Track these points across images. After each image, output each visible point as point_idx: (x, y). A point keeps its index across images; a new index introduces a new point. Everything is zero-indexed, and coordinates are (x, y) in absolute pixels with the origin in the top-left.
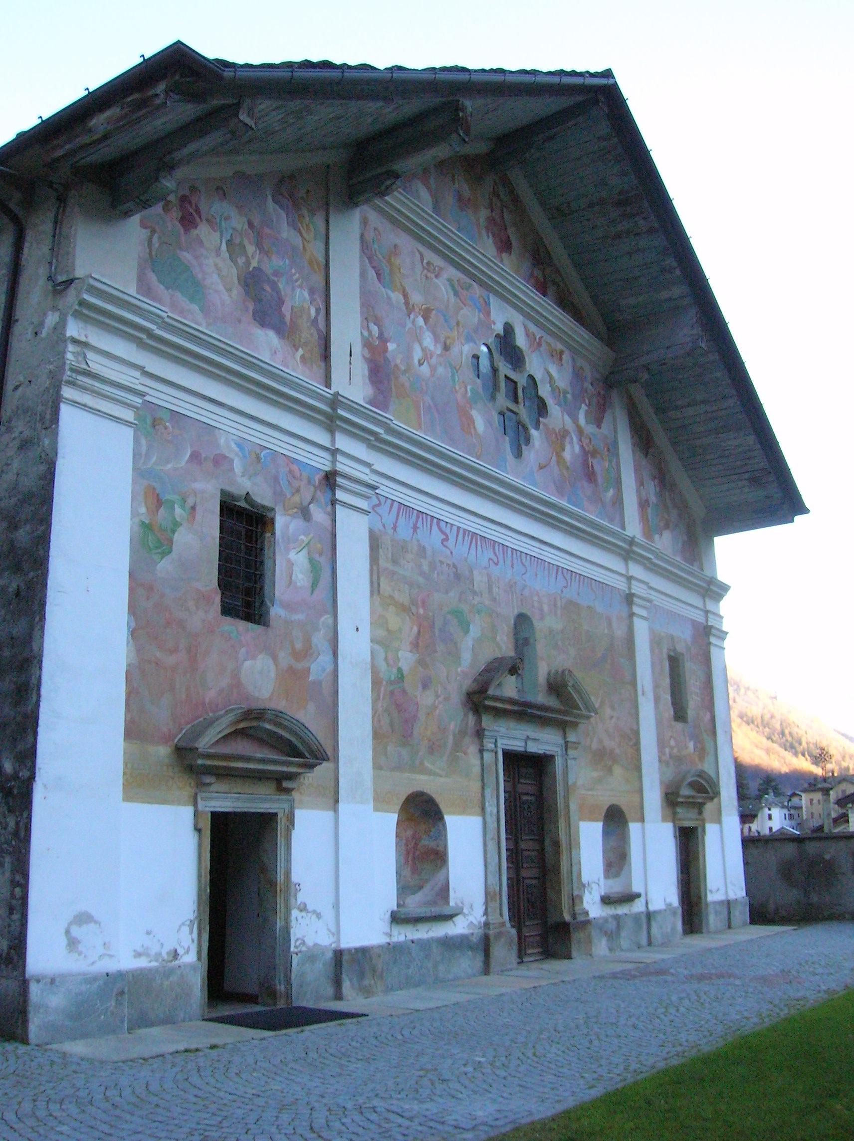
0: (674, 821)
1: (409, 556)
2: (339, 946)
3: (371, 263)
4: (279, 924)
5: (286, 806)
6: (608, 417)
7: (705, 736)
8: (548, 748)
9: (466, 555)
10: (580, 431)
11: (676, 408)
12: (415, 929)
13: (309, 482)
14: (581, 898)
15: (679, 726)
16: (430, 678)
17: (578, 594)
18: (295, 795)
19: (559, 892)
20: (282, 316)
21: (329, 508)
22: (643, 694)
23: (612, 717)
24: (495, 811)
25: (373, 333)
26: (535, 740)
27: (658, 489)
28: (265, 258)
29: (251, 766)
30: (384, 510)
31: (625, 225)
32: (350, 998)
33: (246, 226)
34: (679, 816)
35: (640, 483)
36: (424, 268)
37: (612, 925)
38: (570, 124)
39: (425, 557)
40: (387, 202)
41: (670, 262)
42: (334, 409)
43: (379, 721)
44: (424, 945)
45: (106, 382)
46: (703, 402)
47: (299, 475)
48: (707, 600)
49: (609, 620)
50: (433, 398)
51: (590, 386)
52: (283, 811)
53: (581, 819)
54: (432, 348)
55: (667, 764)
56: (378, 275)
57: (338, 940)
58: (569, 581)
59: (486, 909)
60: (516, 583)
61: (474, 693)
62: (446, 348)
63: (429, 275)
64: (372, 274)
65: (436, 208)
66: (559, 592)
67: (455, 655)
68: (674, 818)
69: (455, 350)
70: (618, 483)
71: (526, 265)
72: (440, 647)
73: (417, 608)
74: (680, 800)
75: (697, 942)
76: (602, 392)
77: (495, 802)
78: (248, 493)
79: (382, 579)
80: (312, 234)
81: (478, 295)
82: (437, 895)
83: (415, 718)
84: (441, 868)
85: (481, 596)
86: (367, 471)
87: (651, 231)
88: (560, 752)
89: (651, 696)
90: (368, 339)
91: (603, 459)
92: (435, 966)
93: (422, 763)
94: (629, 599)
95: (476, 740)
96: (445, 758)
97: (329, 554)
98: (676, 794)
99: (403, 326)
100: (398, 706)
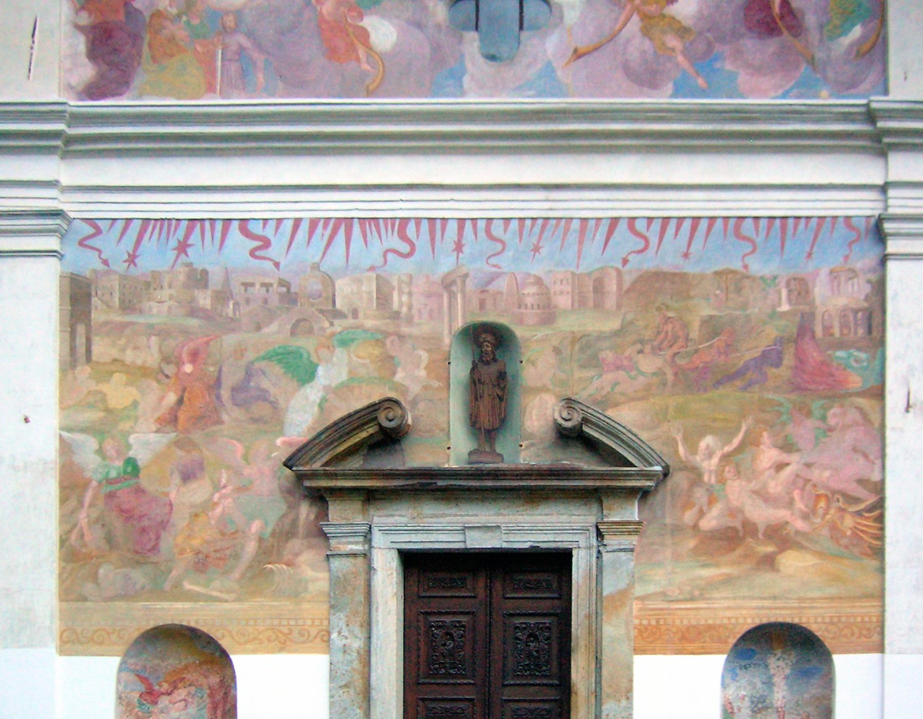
1: (165, 294)
45: (32, 215)
58: (654, 241)
60: (466, 275)
66: (619, 265)
72: (231, 415)
83: (164, 525)
86: (53, 193)
93: (177, 585)
95: (318, 541)
96: (236, 575)
100: (127, 514)
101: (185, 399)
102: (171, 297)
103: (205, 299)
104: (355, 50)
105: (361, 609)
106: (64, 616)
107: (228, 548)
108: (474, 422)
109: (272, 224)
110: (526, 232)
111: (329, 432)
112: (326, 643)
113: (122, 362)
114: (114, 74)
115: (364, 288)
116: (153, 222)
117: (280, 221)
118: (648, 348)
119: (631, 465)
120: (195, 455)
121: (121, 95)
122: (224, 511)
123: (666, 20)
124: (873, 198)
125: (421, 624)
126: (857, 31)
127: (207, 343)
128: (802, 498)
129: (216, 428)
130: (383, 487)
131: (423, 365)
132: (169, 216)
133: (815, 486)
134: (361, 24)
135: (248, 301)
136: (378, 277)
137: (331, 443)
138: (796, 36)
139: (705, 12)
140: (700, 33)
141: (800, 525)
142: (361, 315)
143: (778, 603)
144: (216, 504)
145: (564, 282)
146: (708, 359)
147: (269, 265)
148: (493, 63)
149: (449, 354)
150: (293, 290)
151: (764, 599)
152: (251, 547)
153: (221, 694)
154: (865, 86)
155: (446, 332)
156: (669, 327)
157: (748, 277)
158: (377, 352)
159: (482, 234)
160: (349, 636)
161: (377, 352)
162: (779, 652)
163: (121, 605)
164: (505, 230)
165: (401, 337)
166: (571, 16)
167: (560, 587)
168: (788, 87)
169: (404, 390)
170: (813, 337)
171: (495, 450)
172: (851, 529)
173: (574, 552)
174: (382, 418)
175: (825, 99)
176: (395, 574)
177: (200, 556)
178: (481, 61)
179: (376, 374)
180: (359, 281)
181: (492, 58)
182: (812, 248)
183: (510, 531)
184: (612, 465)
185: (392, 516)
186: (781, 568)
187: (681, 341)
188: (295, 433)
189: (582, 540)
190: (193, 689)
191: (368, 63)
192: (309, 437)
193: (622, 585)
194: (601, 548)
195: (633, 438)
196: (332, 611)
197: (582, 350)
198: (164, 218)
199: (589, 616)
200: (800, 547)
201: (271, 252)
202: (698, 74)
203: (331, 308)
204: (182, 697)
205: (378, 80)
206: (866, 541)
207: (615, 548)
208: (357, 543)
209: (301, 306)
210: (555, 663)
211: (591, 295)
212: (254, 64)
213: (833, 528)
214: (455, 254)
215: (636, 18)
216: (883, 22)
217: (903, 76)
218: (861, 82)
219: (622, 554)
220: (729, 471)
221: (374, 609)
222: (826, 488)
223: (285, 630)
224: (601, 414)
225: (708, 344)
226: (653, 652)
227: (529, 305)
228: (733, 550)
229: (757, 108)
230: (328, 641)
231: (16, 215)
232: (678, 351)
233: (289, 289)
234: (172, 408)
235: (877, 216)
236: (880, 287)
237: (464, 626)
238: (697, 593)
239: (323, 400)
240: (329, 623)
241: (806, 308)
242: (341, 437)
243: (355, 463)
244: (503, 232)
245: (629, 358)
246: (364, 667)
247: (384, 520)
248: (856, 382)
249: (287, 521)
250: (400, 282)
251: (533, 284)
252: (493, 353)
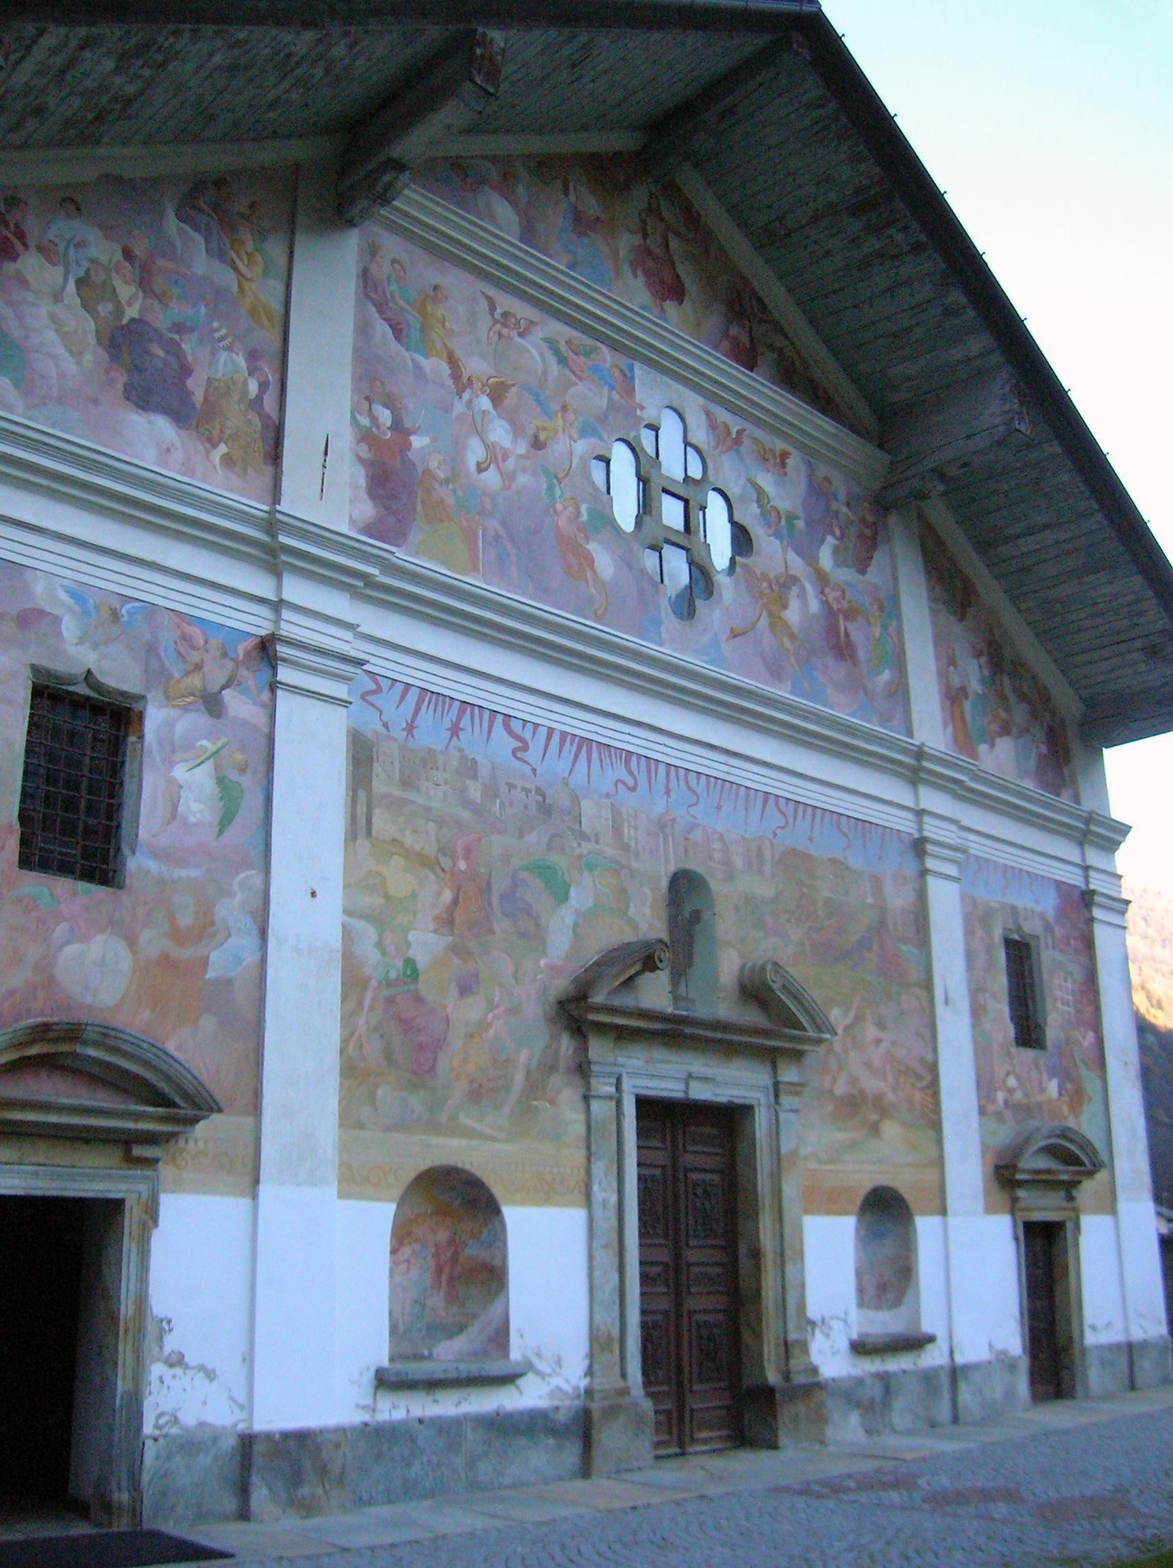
0: (1012, 1212)
1: (440, 776)
2: (252, 1428)
3: (381, 312)
4: (121, 1386)
5: (143, 1188)
6: (880, 558)
7: (1083, 1071)
8: (741, 1093)
9: (566, 775)
10: (822, 579)
11: (1007, 540)
12: (430, 1398)
13: (225, 654)
14: (804, 1347)
15: (1028, 1054)
16: (477, 976)
17: (811, 839)
18: (166, 1171)
19: (758, 1336)
20: (186, 395)
21: (265, 696)
22: (947, 1002)
23: (878, 1041)
24: (614, 1198)
25: (381, 420)
26: (705, 1079)
27: (986, 672)
28: (156, 304)
29: (53, 1118)
30: (387, 701)
31: (872, 244)
32: (266, 1517)
33: (119, 256)
34: (1022, 1204)
35: (948, 661)
36: (495, 322)
37: (876, 1391)
38: (752, 84)
39: (475, 777)
40: (397, 209)
41: (957, 297)
42: (273, 536)
43: (361, 1047)
44: (448, 1429)
46: (1047, 527)
47: (202, 642)
48: (1087, 847)
49: (877, 882)
50: (503, 523)
51: (844, 509)
52: (135, 1196)
53: (808, 1211)
54: (507, 444)
55: (1000, 1118)
56: (398, 332)
57: (250, 1418)
58: (791, 819)
59: (591, 1366)
60: (674, 820)
61: (568, 1001)
62: (537, 444)
63: (505, 331)
64: (382, 329)
65: (528, 233)
66: (770, 836)
67: (535, 937)
68: (1013, 1207)
69: (558, 449)
70: (899, 662)
71: (714, 321)
72: (502, 925)
73: (454, 859)
74: (1019, 1176)
75: (1057, 1416)
76: (870, 518)
77: (615, 1184)
78: (89, 671)
79: (376, 812)
80: (259, 269)
81: (608, 365)
82: (490, 1340)
83: (440, 1043)
84: (497, 1294)
85: (597, 842)
86: (348, 635)
87: (917, 247)
88: (763, 1102)
89: (964, 1006)
90: (370, 429)
91: (869, 623)
92: (471, 1464)
94: (919, 846)
95: (576, 1080)
96: (507, 1110)
97: (262, 769)
98: (1013, 1167)
99: (448, 409)
100: (406, 1024)
106: (344, 1147)
113: (402, 845)
114: (391, 520)
127: (480, 839)
131: (648, 904)
144: (489, 1025)
150: (548, 801)
152: (519, 1078)
153: (449, 1254)
155: (663, 873)
163: (398, 1137)
190: (417, 1247)
194: (777, 1107)
204: (406, 1257)
214: (665, 797)
231: (323, 653)
233: (544, 800)
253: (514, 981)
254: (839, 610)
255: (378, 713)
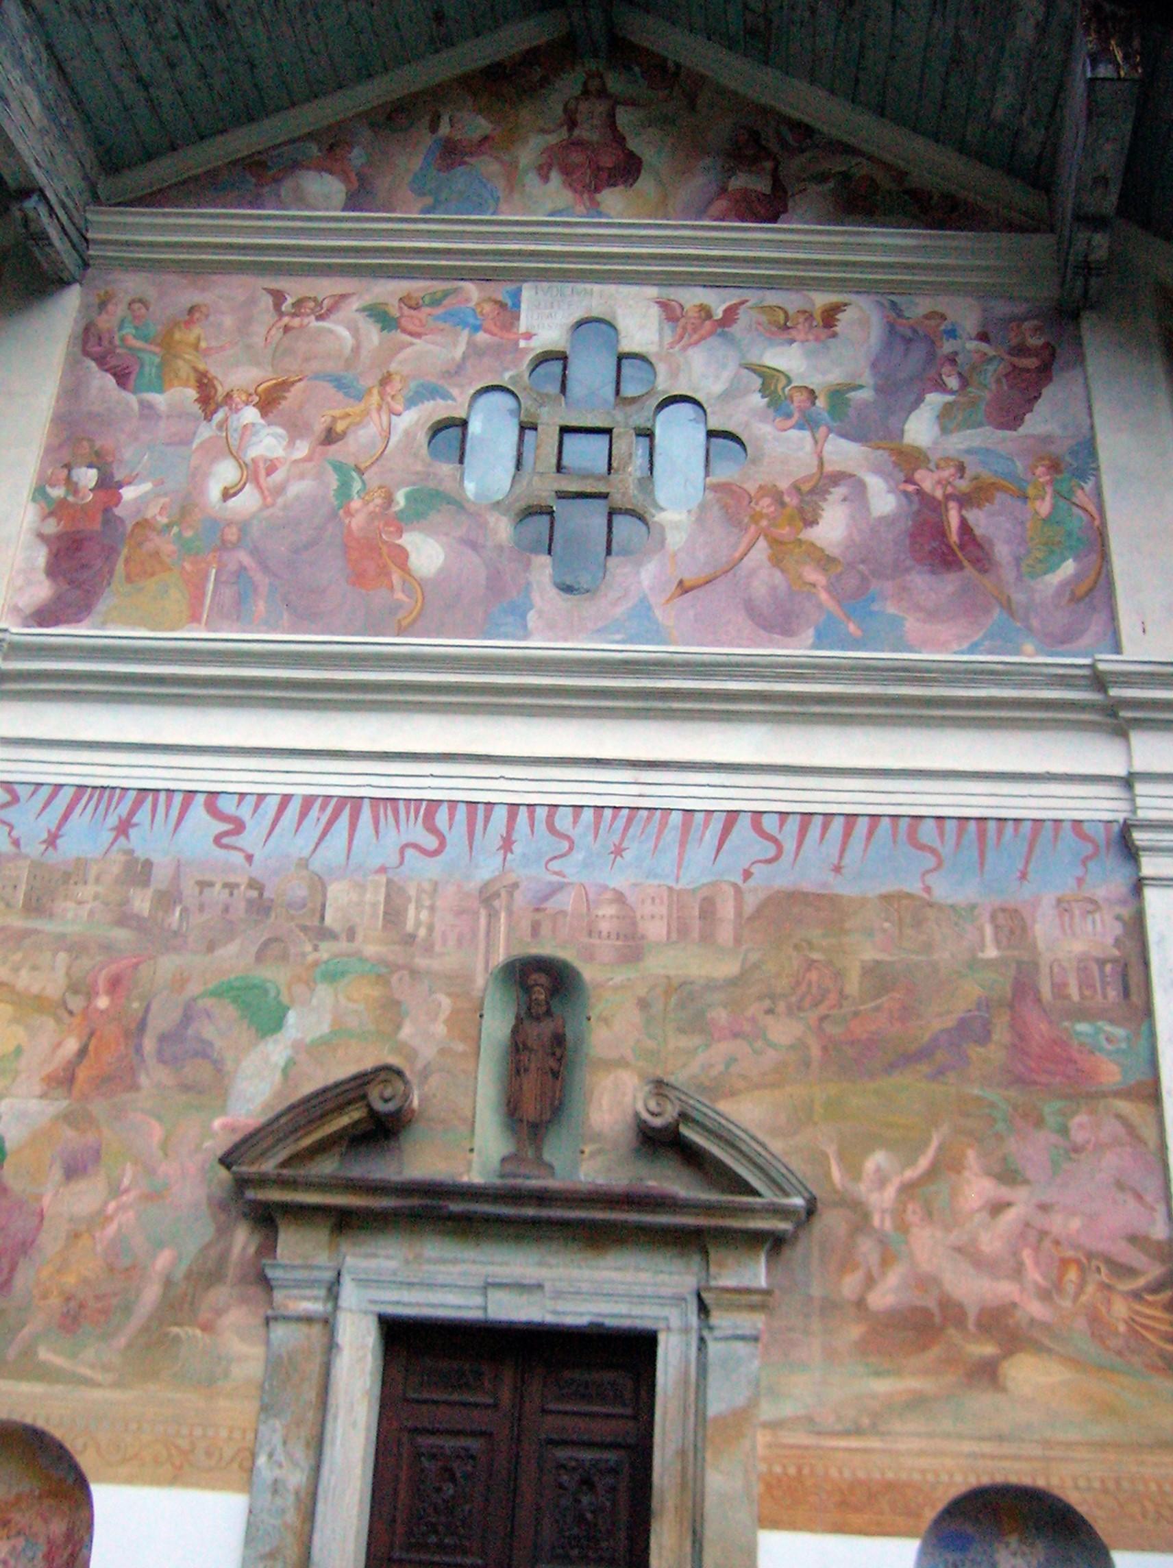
1: (86, 892)
8: (622, 1308)
23: (997, 1208)
56: (122, 378)
58: (789, 845)
60: (515, 885)
66: (738, 879)
72: (153, 1076)
83: (25, 1246)
93: (29, 1352)
95: (255, 1291)
96: (122, 1341)
101: (91, 1048)
102: (96, 897)
103: (142, 901)
104: (388, 575)
105: (310, 1415)
107: (116, 1295)
108: (512, 1110)
109: (250, 801)
110: (604, 826)
111: (291, 1115)
112: (246, 1479)
115: (368, 896)
116: (89, 790)
117: (261, 797)
118: (781, 1006)
119: (754, 1192)
120: (91, 1137)
121: (79, 621)
122: (120, 1226)
123: (804, 547)
124: (1113, 796)
125: (405, 1450)
126: (1069, 567)
128: (1037, 1263)
129: (127, 1096)
130: (367, 1208)
131: (443, 1016)
132: (113, 783)
133: (1057, 1243)
134: (399, 542)
135: (202, 908)
136: (389, 882)
137: (296, 1130)
138: (984, 571)
139: (857, 539)
140: (851, 565)
141: (1036, 1309)
142: (360, 936)
143: (1007, 1449)
144: (109, 1219)
145: (657, 901)
146: (873, 1028)
147: (237, 858)
148: (568, 596)
149: (482, 1004)
150: (266, 895)
151: (983, 1439)
152: (151, 1294)
153: (66, 1555)
154: (1086, 640)
155: (480, 966)
156: (814, 976)
157: (931, 905)
158: (376, 992)
159: (541, 826)
160: (284, 1464)
161: (376, 992)
162: (1013, 1540)
164: (575, 822)
165: (414, 973)
166: (675, 540)
167: (636, 1392)
168: (976, 638)
169: (412, 1055)
170: (1038, 1000)
171: (541, 1155)
172: (1127, 1323)
173: (662, 1338)
174: (374, 1094)
175: (1030, 655)
176: (370, 1358)
177: (72, 1304)
178: (553, 592)
179: (372, 1027)
180: (362, 887)
181: (568, 589)
182: (1027, 862)
183: (558, 1295)
184: (723, 1191)
185: (375, 1256)
186: (1010, 1385)
187: (833, 997)
188: (243, 1112)
189: (674, 1316)
190: (20, 1543)
191: (403, 591)
192: (263, 1120)
193: (740, 1401)
194: (705, 1333)
195: (759, 1149)
196: (262, 1417)
197: (682, 1005)
198: (106, 785)
199: (682, 1453)
200: (1039, 1348)
201: (244, 840)
202: (849, 618)
203: (316, 923)
205: (414, 614)
206: (1152, 1344)
207: (729, 1332)
208: (316, 1299)
209: (276, 917)
210: (622, 1535)
211: (696, 924)
212: (255, 590)
213: (1094, 1319)
215: (762, 544)
216: (1105, 556)
217: (1141, 630)
218: (1082, 633)
219: (739, 1345)
220: (913, 1213)
221: (330, 1418)
222: (1077, 1247)
223: (184, 1443)
224: (708, 1107)
225: (873, 1004)
226: (793, 1526)
227: (604, 934)
228: (924, 1348)
229: (935, 665)
230: (251, 1470)
232: (827, 1012)
233: (261, 895)
234: (70, 1062)
235: (1121, 821)
236: (1137, 926)
237: (472, 1457)
238: (866, 1421)
239: (291, 1063)
240: (256, 1438)
241: (1026, 957)
242: (310, 1122)
243: (327, 1166)
244: (571, 825)
245: (753, 1020)
246: (304, 1522)
247: (364, 1263)
248: (1111, 1074)
249: (213, 1253)
250: (420, 890)
251: (611, 902)
252: (547, 1003)
253: (161, 1154)
254: (948, 497)
255: (7, 829)
